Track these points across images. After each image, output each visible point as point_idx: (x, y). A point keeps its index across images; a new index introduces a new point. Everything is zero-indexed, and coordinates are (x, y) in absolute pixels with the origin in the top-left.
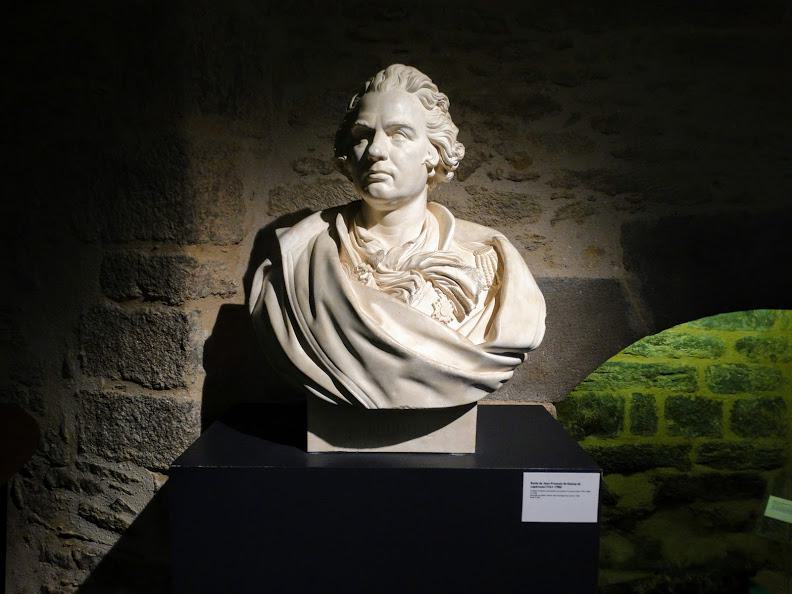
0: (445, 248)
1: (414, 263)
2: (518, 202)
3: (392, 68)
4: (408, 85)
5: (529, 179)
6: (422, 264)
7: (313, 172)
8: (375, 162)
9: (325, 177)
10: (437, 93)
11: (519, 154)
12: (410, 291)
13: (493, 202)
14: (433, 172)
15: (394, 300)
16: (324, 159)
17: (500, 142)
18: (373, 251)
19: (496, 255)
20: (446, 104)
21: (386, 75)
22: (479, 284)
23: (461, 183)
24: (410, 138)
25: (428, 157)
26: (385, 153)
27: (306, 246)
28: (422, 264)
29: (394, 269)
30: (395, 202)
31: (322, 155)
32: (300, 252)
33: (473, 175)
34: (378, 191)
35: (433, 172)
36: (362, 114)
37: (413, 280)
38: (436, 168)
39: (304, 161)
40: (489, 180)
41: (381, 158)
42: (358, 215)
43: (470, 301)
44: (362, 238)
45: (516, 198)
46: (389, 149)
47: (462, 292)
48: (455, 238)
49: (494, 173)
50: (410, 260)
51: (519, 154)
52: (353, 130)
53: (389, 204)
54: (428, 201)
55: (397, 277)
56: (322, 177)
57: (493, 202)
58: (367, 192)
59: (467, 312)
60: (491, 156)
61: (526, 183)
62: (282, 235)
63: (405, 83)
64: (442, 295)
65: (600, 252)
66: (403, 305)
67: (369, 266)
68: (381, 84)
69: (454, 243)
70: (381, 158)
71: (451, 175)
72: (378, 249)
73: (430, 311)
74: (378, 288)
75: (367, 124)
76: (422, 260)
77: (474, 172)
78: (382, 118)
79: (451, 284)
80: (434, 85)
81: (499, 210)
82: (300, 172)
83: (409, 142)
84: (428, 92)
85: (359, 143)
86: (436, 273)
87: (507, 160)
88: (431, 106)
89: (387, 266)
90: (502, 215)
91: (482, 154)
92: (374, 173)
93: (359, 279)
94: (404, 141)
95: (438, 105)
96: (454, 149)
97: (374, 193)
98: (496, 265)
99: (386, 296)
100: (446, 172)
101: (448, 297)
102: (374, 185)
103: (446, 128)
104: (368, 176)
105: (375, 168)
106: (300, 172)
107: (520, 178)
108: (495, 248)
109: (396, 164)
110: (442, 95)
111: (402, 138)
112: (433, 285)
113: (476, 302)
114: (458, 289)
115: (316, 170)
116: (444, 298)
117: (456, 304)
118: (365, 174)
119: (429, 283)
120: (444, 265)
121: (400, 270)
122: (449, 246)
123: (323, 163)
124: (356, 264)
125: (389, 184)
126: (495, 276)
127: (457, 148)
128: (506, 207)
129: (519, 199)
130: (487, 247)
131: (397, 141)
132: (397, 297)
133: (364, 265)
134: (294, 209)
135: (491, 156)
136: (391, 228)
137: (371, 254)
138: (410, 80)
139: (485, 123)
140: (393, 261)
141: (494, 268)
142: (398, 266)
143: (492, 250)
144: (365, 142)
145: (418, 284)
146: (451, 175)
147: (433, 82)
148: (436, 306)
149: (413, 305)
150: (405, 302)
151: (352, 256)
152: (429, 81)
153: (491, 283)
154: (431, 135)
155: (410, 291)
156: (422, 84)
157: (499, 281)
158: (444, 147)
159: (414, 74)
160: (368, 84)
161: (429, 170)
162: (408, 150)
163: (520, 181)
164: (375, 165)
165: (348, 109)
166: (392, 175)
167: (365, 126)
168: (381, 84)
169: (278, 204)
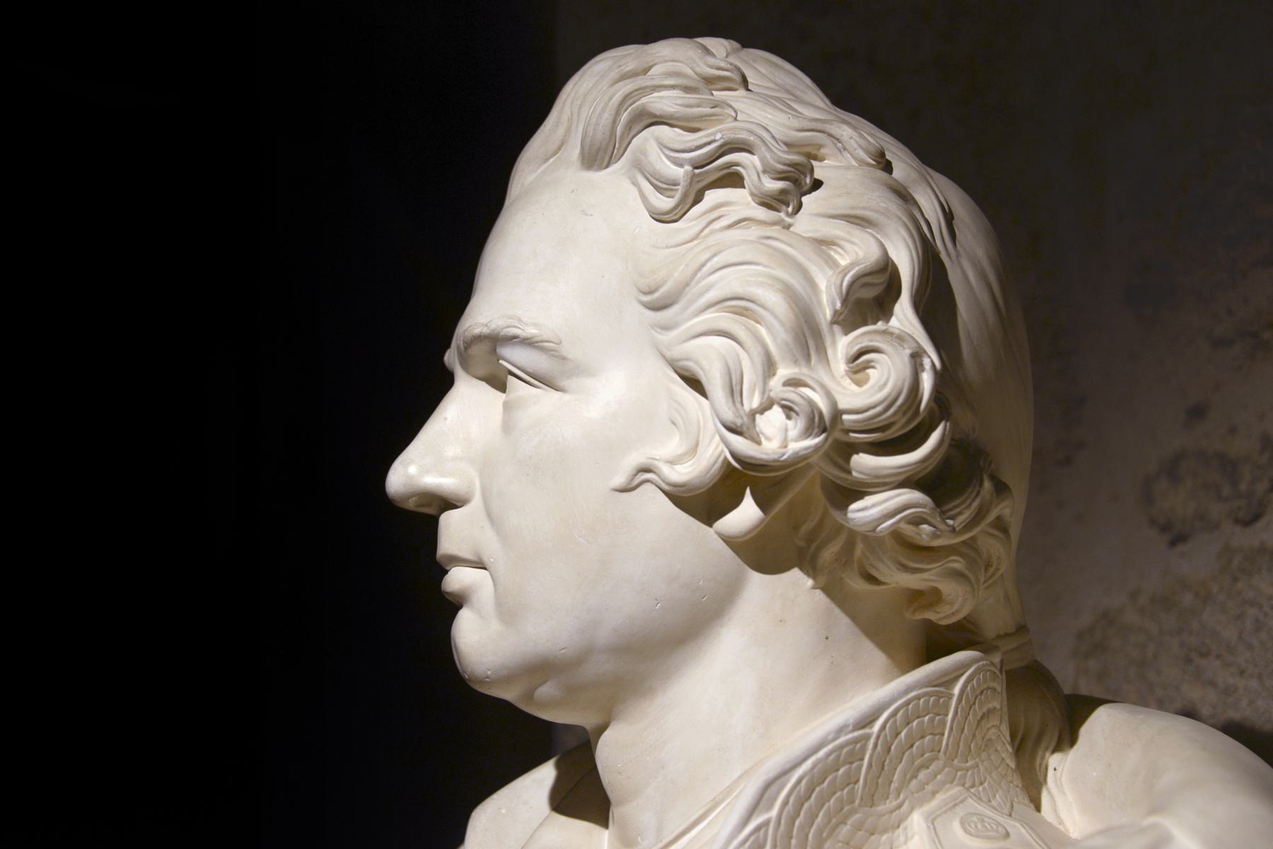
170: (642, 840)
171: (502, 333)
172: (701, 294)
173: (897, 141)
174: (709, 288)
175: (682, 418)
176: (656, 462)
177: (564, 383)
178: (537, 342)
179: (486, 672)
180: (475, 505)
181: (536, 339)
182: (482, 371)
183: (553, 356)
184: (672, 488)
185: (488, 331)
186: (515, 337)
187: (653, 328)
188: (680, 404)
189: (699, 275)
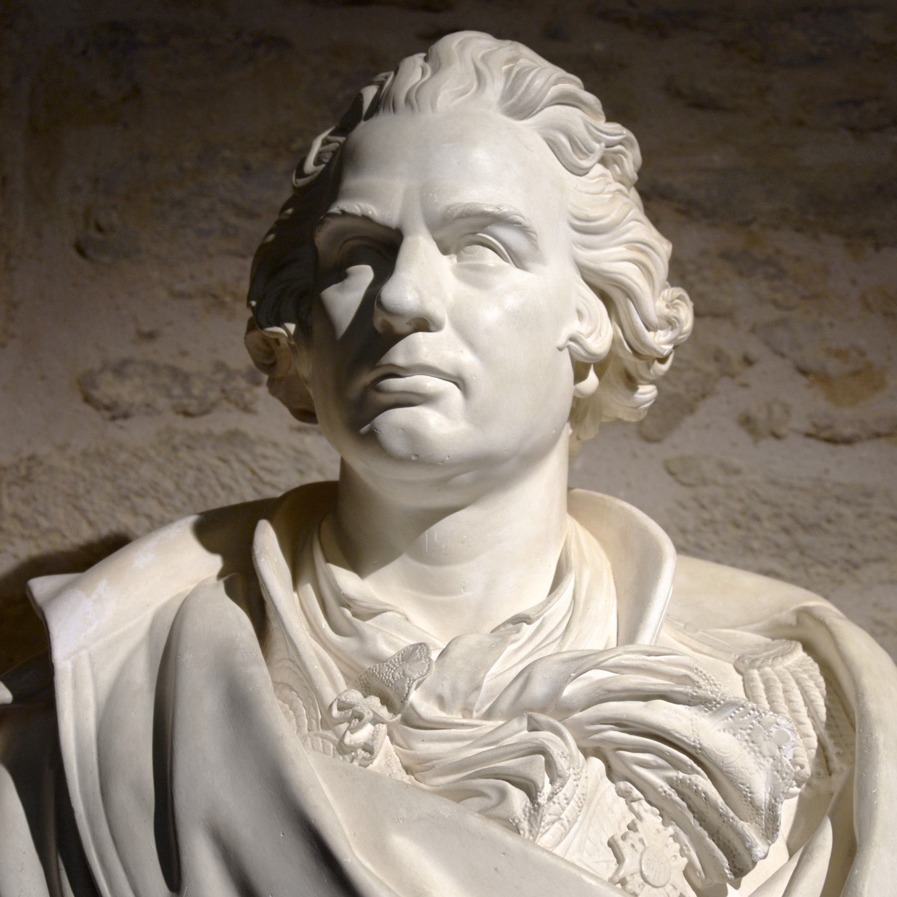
0: (646, 639)
1: (539, 689)
2: (848, 512)
3: (453, 42)
4: (509, 92)
5: (878, 435)
6: (569, 690)
7: (150, 409)
8: (398, 337)
9: (190, 425)
10: (602, 123)
11: (839, 354)
12: (530, 790)
13: (764, 511)
14: (592, 381)
15: (475, 821)
16: (188, 365)
17: (777, 314)
18: (388, 651)
19: (815, 669)
20: (632, 159)
21: (437, 66)
22: (777, 769)
23: (654, 448)
24: (517, 260)
25: (575, 327)
26: (436, 308)
27: (141, 632)
28: (569, 690)
29: (467, 710)
30: (465, 477)
31: (184, 354)
32: (121, 654)
33: (689, 420)
34: (412, 435)
35: (592, 381)
36: (351, 182)
37: (542, 751)
38: (601, 367)
39: (120, 370)
40: (742, 436)
41: (424, 324)
42: (326, 527)
43: (750, 830)
44: (345, 602)
45: (838, 499)
46: (450, 297)
47: (720, 801)
48: (669, 618)
49: (761, 416)
50: (526, 676)
51: (839, 354)
52: (322, 237)
53: (443, 483)
54: (569, 489)
55: (477, 741)
56: (182, 423)
57: (764, 511)
58: (372, 439)
59: (739, 871)
60: (748, 361)
61: (865, 451)
62: (58, 593)
63: (495, 88)
64: (643, 807)
65: (824, 839)
66: (510, 839)
67: (375, 701)
68: (420, 87)
69: (669, 638)
70: (424, 324)
71: (647, 393)
72: (406, 642)
73: (605, 865)
74: (406, 778)
75: (374, 211)
76: (568, 679)
77: (692, 411)
78: (426, 191)
79: (676, 765)
80: (590, 98)
81: (783, 539)
82: (108, 408)
83: (514, 274)
84: (574, 117)
85: (339, 274)
86: (621, 724)
87: (804, 372)
88: (585, 163)
89: (441, 702)
90: (794, 556)
91: (718, 357)
92: (396, 372)
93: (342, 749)
94: (496, 270)
95: (603, 161)
96: (661, 305)
97: (397, 444)
98: (823, 711)
99: (446, 808)
100: (631, 382)
101: (667, 817)
102: (399, 415)
103: (629, 236)
104: (374, 386)
105: (398, 355)
106: (108, 408)
107: (848, 431)
108: (808, 648)
109: (472, 345)
110: (617, 131)
111: (490, 258)
112: (610, 773)
113: (770, 831)
114: (703, 782)
115: (162, 402)
116: (651, 818)
117: (697, 841)
118: (366, 378)
119: (597, 764)
120: (647, 696)
121: (489, 715)
122: (656, 635)
123: (181, 377)
124: (329, 695)
125: (446, 413)
126: (822, 747)
127: (671, 305)
128: (808, 528)
129: (848, 502)
130: (783, 645)
131: (478, 268)
132: (484, 812)
133: (355, 696)
134: (85, 534)
135: (748, 361)
136: (447, 569)
137: (378, 659)
138: (514, 80)
139: (725, 255)
140: (463, 685)
141: (812, 715)
142: (482, 703)
143: (799, 654)
144: (364, 274)
145: (562, 763)
146: (647, 393)
147: (588, 89)
148: (625, 848)
149: (545, 840)
150: (517, 830)
151: (315, 667)
152: (573, 85)
153: (808, 770)
154: (586, 256)
155: (530, 790)
156: (553, 91)
157: (836, 763)
158: (629, 293)
159: (523, 62)
160: (369, 93)
161: (580, 374)
162: (511, 302)
163: (848, 441)
164: (400, 346)
165: (301, 174)
166: (459, 381)
167: (366, 218)
168: (420, 87)
169: (25, 511)
170: (464, 591)
171: (511, 217)
172: (624, 233)
173: (315, 159)
174: (628, 230)
175: (588, 309)
176: (581, 336)
177: (528, 264)
178: (530, 232)
179: (445, 458)
180: (447, 331)
181: (530, 229)
182: (439, 235)
183: (533, 244)
184: (588, 355)
185: (499, 213)
186: (518, 223)
187: (576, 245)
188: (587, 300)
189: (624, 221)
